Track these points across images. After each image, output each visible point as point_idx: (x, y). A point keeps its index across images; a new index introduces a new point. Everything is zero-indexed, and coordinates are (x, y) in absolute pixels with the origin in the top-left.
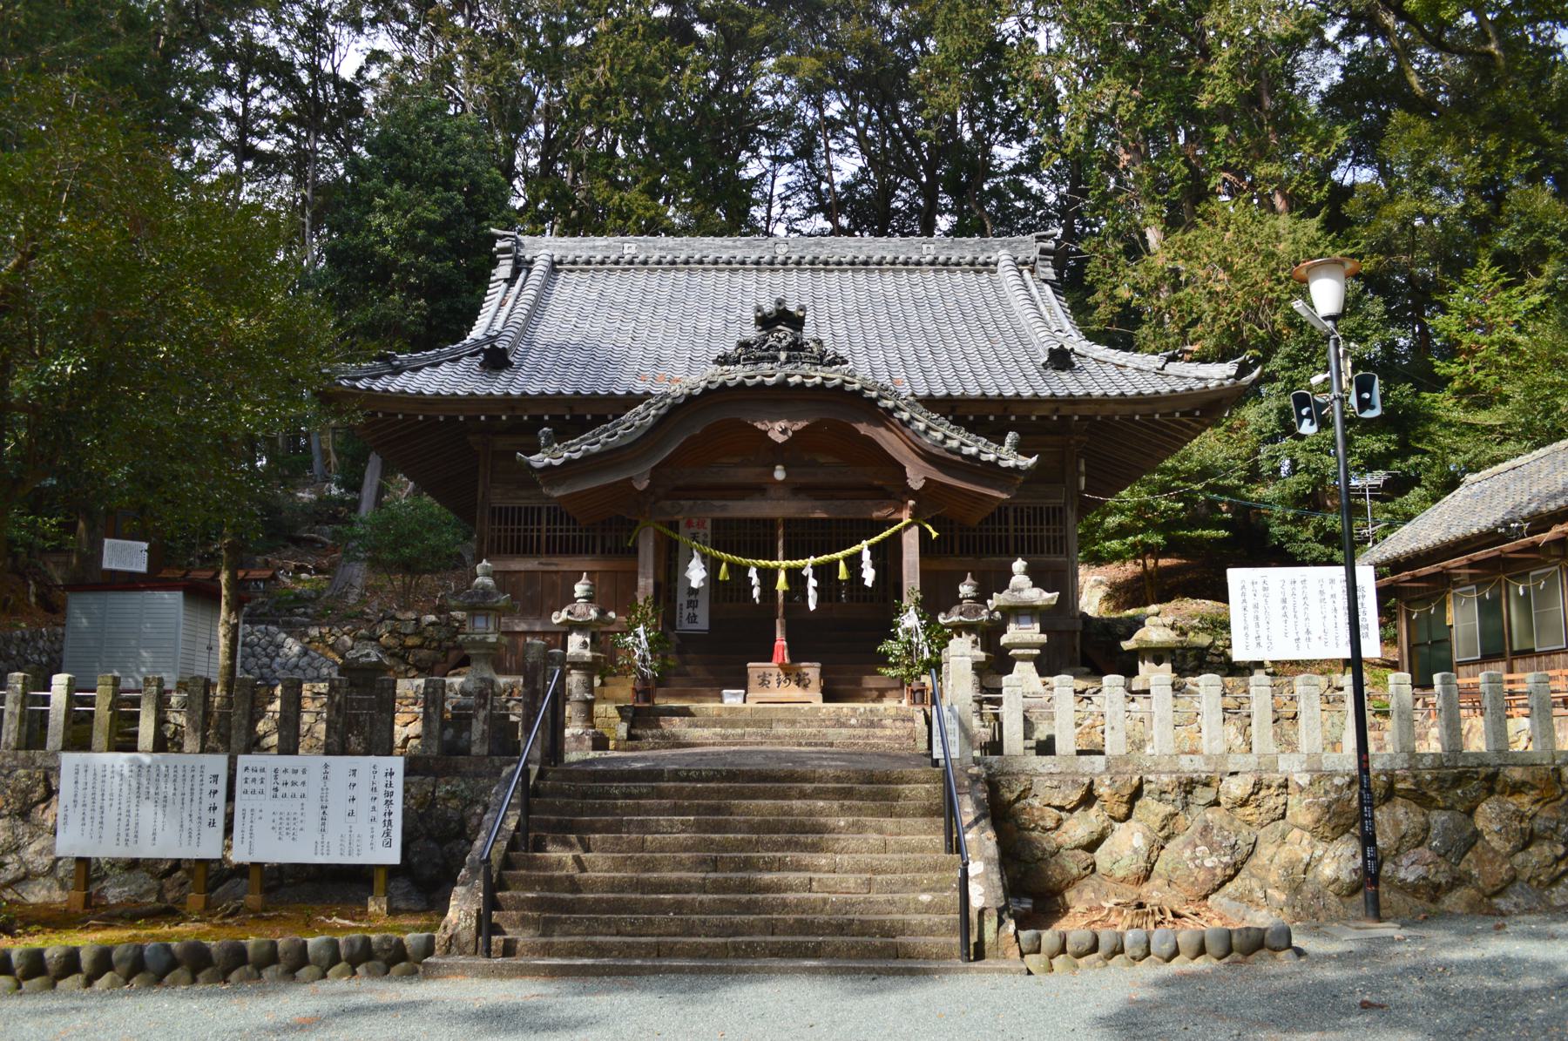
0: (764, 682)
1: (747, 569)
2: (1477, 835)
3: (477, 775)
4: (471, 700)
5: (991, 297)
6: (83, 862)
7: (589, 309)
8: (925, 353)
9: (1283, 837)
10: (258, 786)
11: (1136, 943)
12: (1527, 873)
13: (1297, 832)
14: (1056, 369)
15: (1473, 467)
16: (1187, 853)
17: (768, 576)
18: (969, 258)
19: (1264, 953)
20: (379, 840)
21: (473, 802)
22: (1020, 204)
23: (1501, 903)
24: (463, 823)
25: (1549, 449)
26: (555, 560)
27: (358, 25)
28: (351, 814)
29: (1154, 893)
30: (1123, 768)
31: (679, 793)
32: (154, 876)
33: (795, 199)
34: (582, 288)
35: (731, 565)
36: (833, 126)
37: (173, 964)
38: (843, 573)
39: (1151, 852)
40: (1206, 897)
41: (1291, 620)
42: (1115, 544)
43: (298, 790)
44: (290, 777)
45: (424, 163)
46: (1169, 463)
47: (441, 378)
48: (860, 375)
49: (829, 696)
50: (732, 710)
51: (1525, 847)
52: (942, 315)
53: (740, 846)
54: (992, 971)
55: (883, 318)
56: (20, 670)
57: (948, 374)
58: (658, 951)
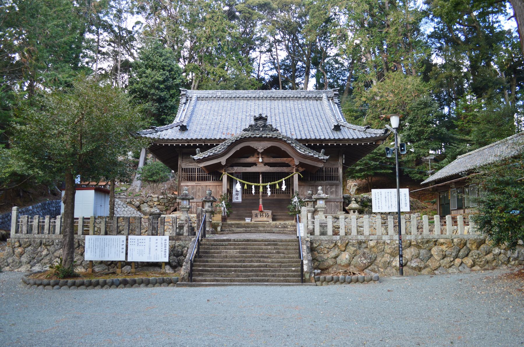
0: (256, 216)
1: (252, 186)
2: (432, 255)
3: (185, 240)
4: (184, 222)
5: (320, 108)
6: (91, 261)
7: (208, 112)
8: (300, 125)
9: (383, 256)
10: (133, 243)
11: (342, 279)
12: (443, 265)
13: (387, 255)
14: (336, 130)
15: (461, 153)
16: (359, 259)
17: (257, 188)
18: (314, 96)
19: (372, 281)
20: (163, 256)
21: (185, 247)
22: (337, 66)
23: (436, 272)
24: (182, 252)
25: (479, 149)
26: (199, 182)
27: (132, 13)
28: (156, 250)
29: (351, 269)
30: (344, 239)
31: (235, 245)
32: (106, 265)
33: (267, 65)
34: (206, 105)
35: (247, 185)
36: (279, 41)
37: (120, 283)
38: (278, 187)
39: (350, 259)
40: (363, 270)
41: (387, 202)
42: (359, 175)
43: (143, 244)
44: (141, 241)
45: (157, 63)
46: (375, 151)
47: (169, 133)
48: (282, 134)
49: (274, 219)
50: (248, 223)
51: (443, 258)
52: (306, 115)
53: (250, 257)
54: (308, 285)
55: (289, 115)
56: (15, 206)
57: (307, 132)
58: (231, 281)
